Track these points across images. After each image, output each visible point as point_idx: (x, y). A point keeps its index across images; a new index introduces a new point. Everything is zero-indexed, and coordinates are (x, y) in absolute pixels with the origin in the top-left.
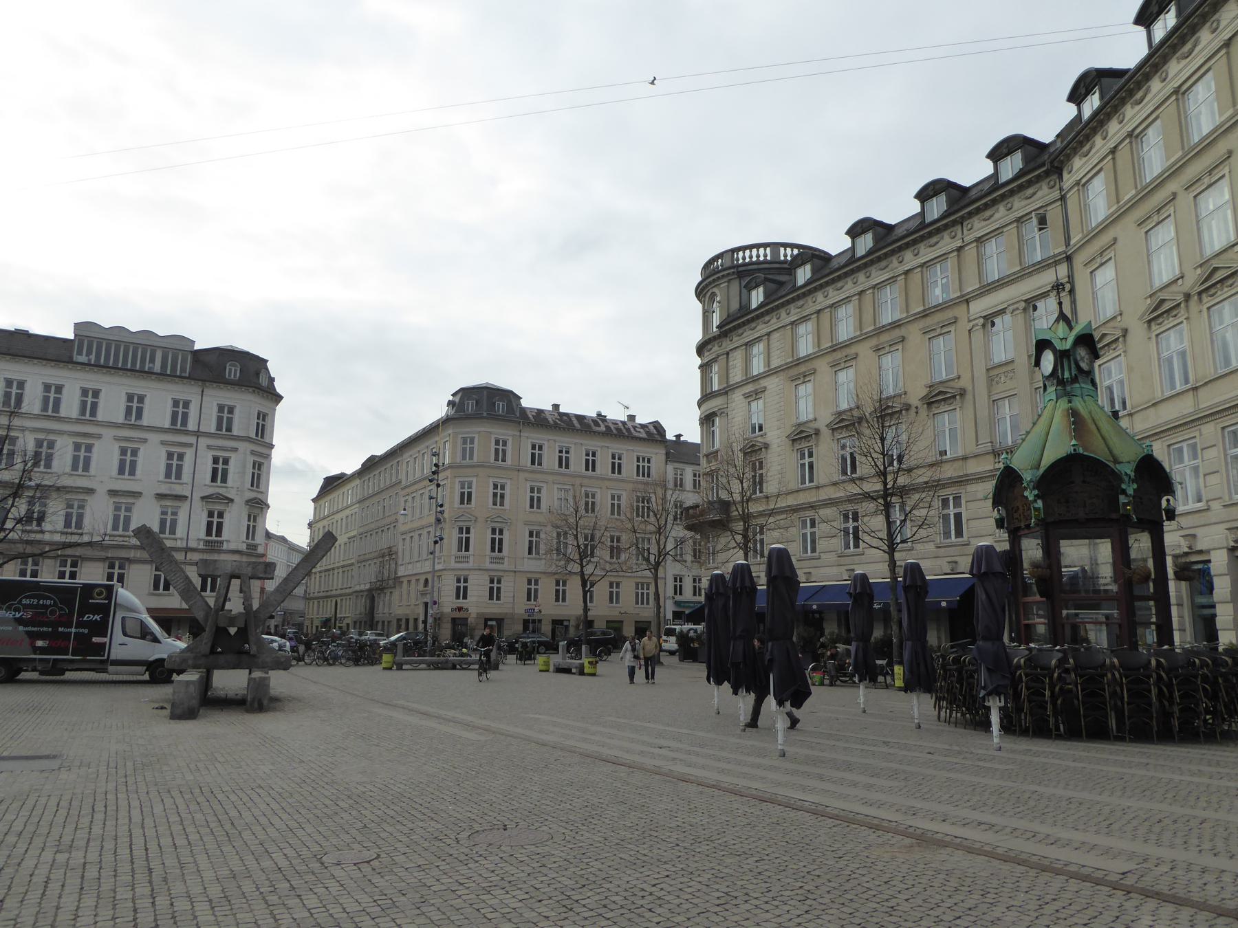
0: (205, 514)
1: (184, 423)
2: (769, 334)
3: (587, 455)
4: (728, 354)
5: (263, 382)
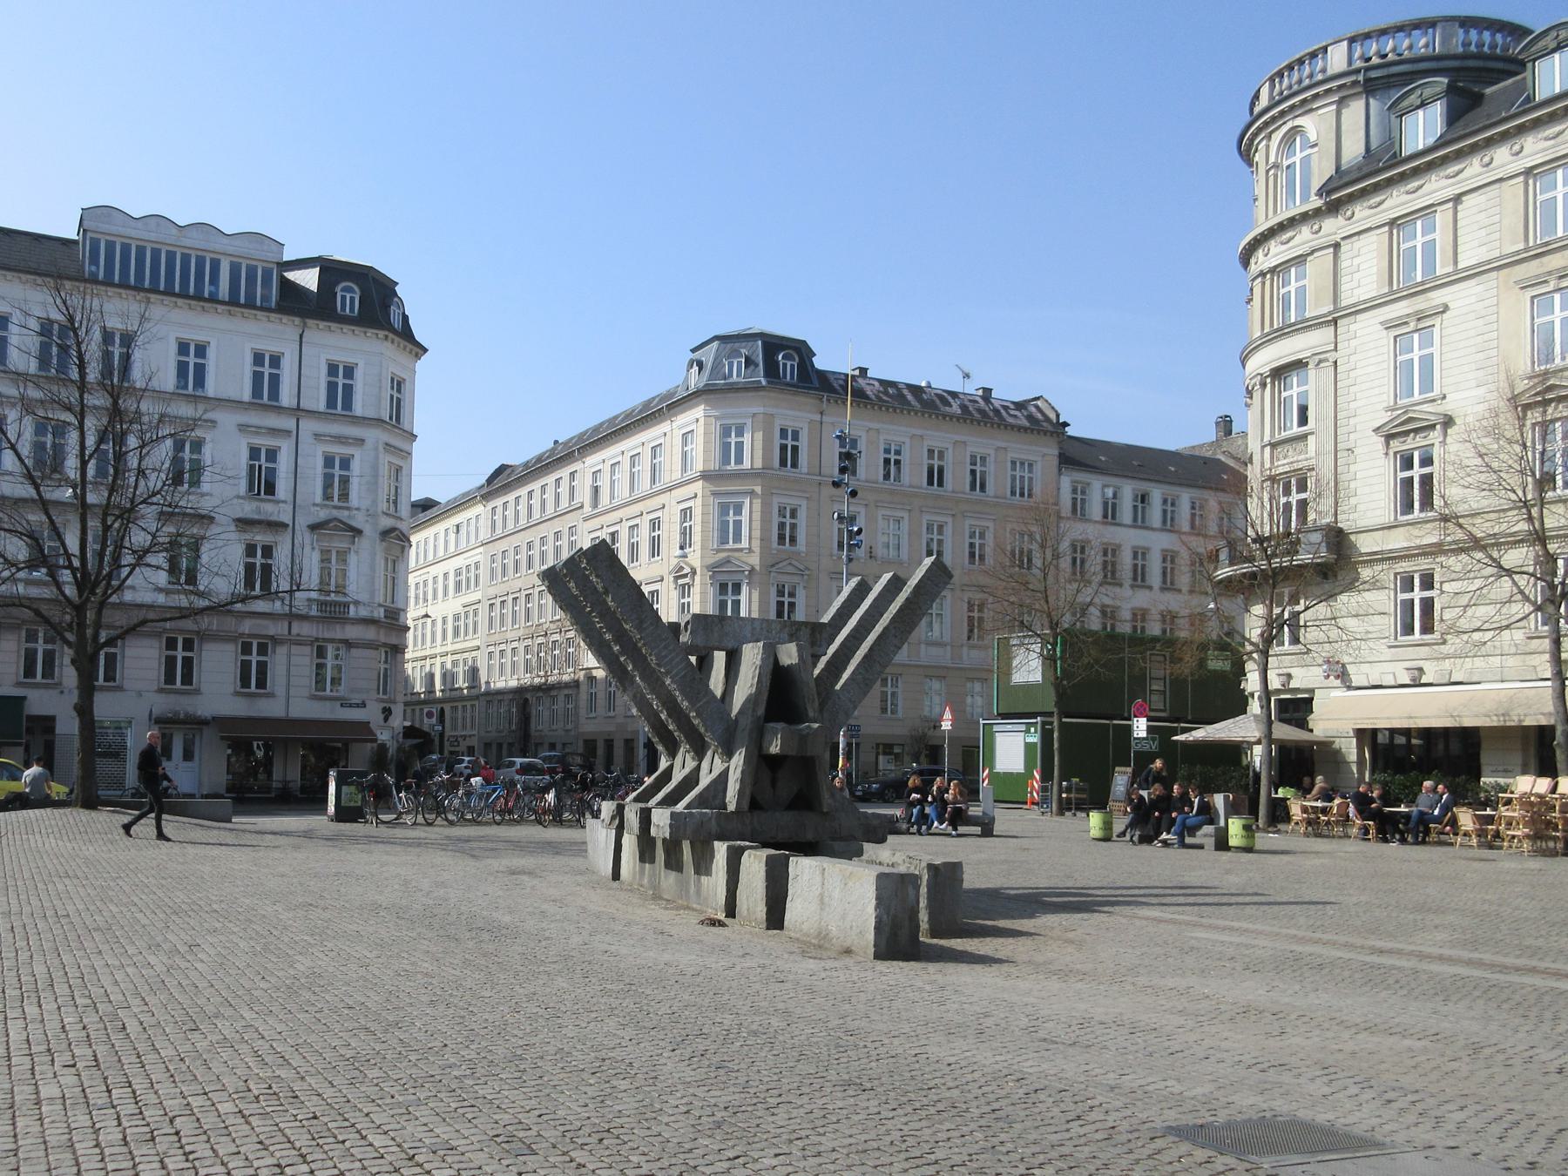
2: (1457, 199)
4: (1337, 246)
5: (398, 324)
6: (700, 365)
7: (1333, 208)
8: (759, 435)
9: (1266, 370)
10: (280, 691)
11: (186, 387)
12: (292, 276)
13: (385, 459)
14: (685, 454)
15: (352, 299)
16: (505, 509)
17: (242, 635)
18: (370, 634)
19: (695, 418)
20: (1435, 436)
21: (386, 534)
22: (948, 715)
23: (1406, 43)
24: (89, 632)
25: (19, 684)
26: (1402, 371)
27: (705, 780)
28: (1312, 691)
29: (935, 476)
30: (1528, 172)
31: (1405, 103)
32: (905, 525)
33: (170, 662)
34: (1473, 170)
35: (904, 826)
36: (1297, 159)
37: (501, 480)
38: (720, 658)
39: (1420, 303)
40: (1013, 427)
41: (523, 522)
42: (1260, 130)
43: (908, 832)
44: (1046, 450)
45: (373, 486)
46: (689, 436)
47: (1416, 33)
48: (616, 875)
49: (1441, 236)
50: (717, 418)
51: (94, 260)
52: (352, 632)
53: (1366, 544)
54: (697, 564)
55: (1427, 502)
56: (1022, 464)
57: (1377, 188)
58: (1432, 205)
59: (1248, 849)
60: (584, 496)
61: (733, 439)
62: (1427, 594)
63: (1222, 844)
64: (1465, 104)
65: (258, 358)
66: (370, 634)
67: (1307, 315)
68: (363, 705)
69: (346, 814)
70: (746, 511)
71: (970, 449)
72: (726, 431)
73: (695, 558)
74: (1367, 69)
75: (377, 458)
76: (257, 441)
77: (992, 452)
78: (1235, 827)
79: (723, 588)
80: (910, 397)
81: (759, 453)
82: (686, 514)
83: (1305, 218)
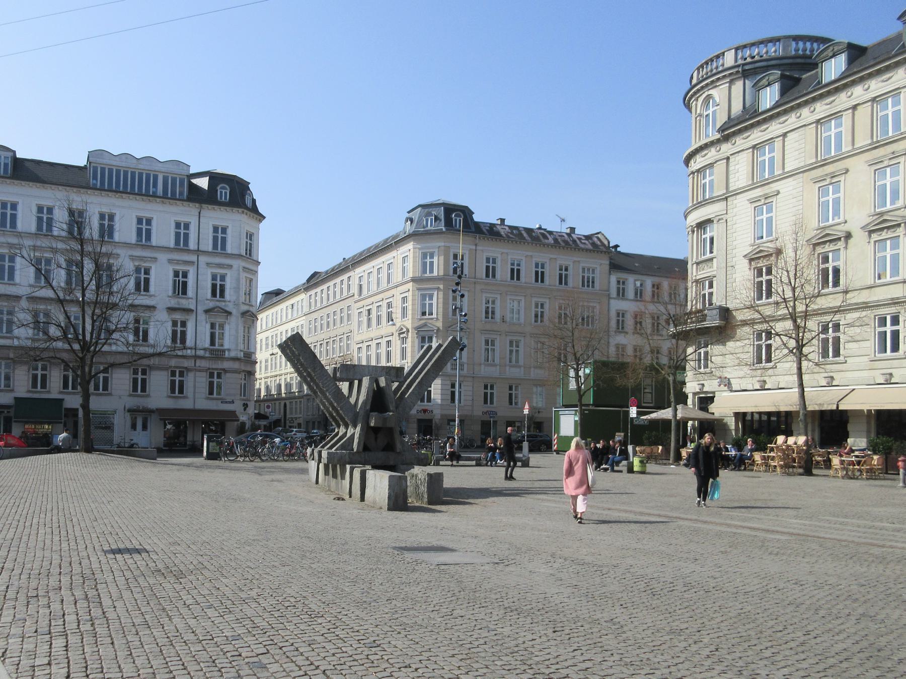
0: (208, 326)
1: (186, 242)
2: (784, 135)
3: (561, 269)
4: (728, 159)
5: (249, 203)
6: (412, 220)
7: (726, 139)
8: (442, 258)
9: (694, 224)
10: (190, 395)
11: (141, 241)
12: (195, 181)
13: (243, 275)
14: (404, 268)
15: (226, 193)
16: (316, 296)
17: (171, 367)
18: (236, 365)
19: (408, 248)
20: (841, 244)
21: (244, 314)
22: (527, 406)
23: (764, 50)
24: (87, 369)
25: (61, 393)
26: (758, 224)
27: (349, 435)
28: (714, 393)
29: (540, 277)
30: (818, 122)
31: (761, 83)
32: (522, 304)
33: (135, 381)
34: (792, 120)
35: (485, 462)
36: (710, 112)
37: (315, 280)
38: (356, 382)
39: (767, 190)
40: (583, 250)
41: (325, 303)
42: (692, 96)
43: (486, 465)
44: (603, 262)
45: (237, 289)
46: (405, 260)
47: (770, 45)
48: (317, 482)
49: (777, 154)
50: (419, 249)
51: (95, 178)
52: (226, 365)
53: (739, 316)
54: (410, 327)
55: (836, 283)
56: (589, 270)
57: (746, 129)
58: (899, 88)
59: (643, 472)
60: (355, 290)
61: (428, 260)
62: (895, 328)
63: (630, 470)
64: (789, 85)
65: (178, 225)
66: (236, 365)
67: (715, 195)
68: (233, 402)
69: (212, 456)
70: (435, 298)
71: (559, 262)
72: (424, 256)
73: (408, 323)
74: (744, 65)
75: (239, 274)
76: (178, 267)
77: (571, 264)
78: (636, 462)
79: (423, 340)
80: (525, 235)
81: (442, 267)
82: (404, 299)
83: (712, 144)
